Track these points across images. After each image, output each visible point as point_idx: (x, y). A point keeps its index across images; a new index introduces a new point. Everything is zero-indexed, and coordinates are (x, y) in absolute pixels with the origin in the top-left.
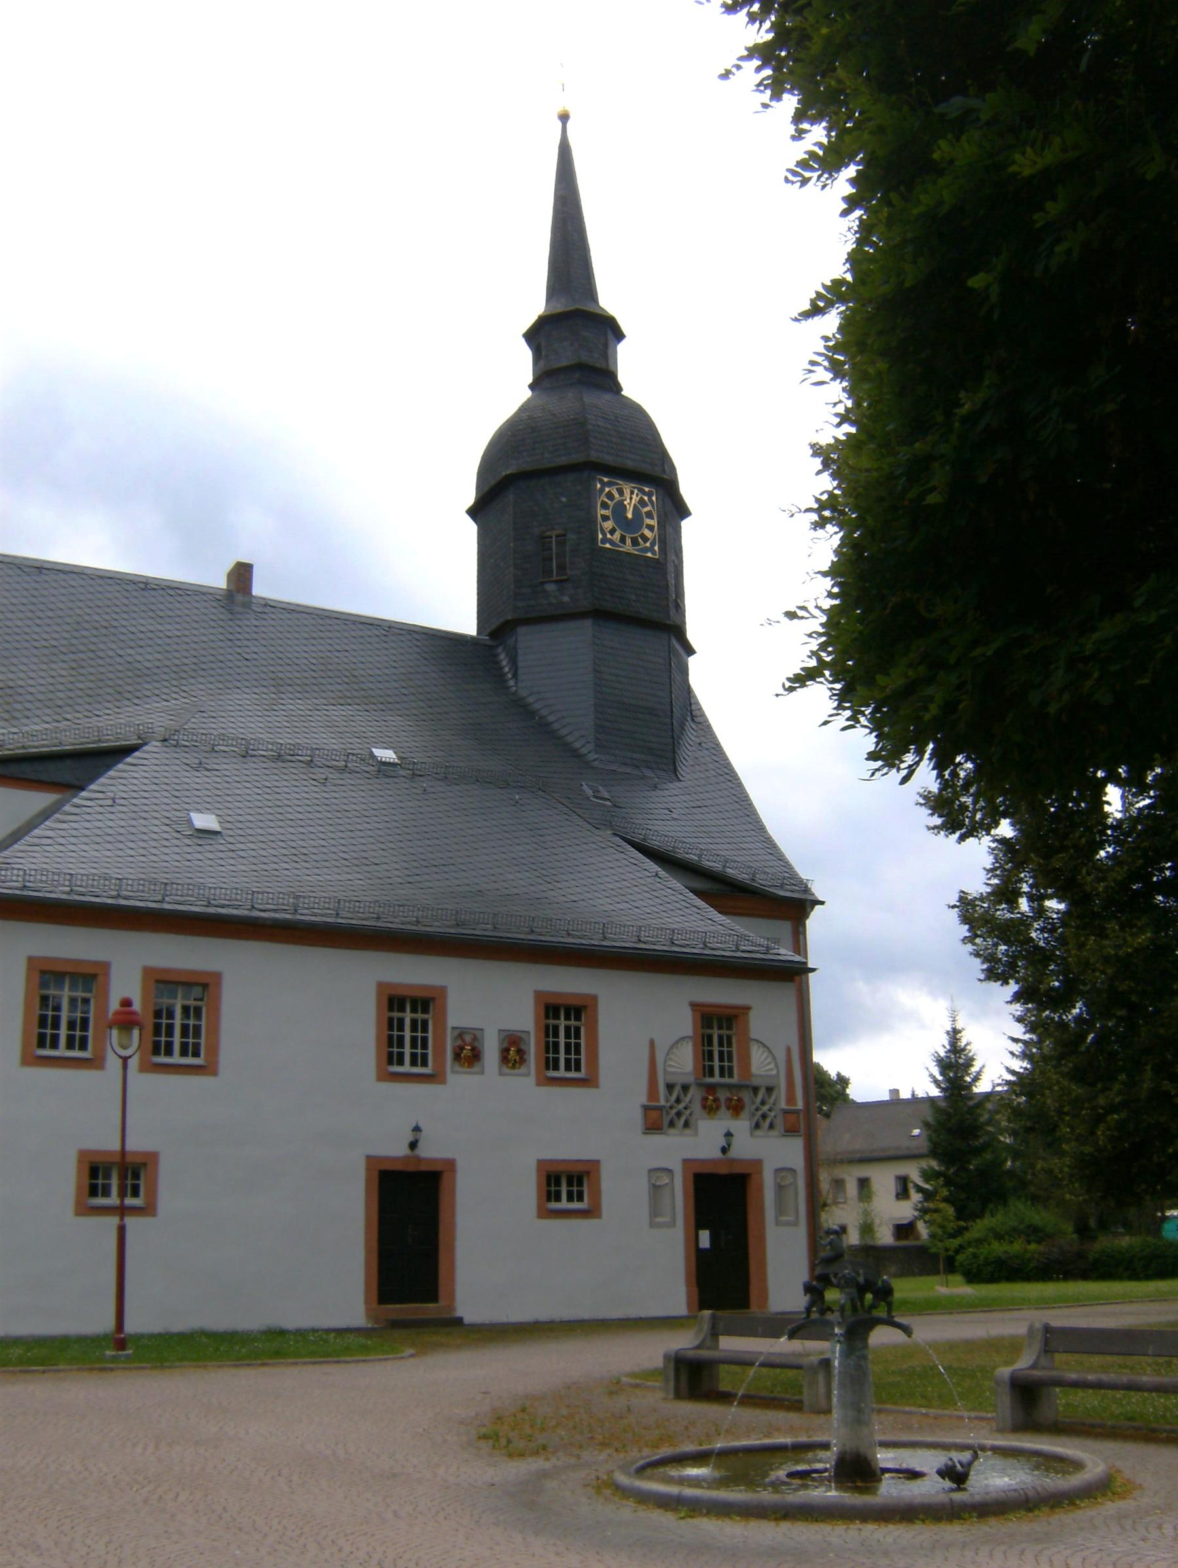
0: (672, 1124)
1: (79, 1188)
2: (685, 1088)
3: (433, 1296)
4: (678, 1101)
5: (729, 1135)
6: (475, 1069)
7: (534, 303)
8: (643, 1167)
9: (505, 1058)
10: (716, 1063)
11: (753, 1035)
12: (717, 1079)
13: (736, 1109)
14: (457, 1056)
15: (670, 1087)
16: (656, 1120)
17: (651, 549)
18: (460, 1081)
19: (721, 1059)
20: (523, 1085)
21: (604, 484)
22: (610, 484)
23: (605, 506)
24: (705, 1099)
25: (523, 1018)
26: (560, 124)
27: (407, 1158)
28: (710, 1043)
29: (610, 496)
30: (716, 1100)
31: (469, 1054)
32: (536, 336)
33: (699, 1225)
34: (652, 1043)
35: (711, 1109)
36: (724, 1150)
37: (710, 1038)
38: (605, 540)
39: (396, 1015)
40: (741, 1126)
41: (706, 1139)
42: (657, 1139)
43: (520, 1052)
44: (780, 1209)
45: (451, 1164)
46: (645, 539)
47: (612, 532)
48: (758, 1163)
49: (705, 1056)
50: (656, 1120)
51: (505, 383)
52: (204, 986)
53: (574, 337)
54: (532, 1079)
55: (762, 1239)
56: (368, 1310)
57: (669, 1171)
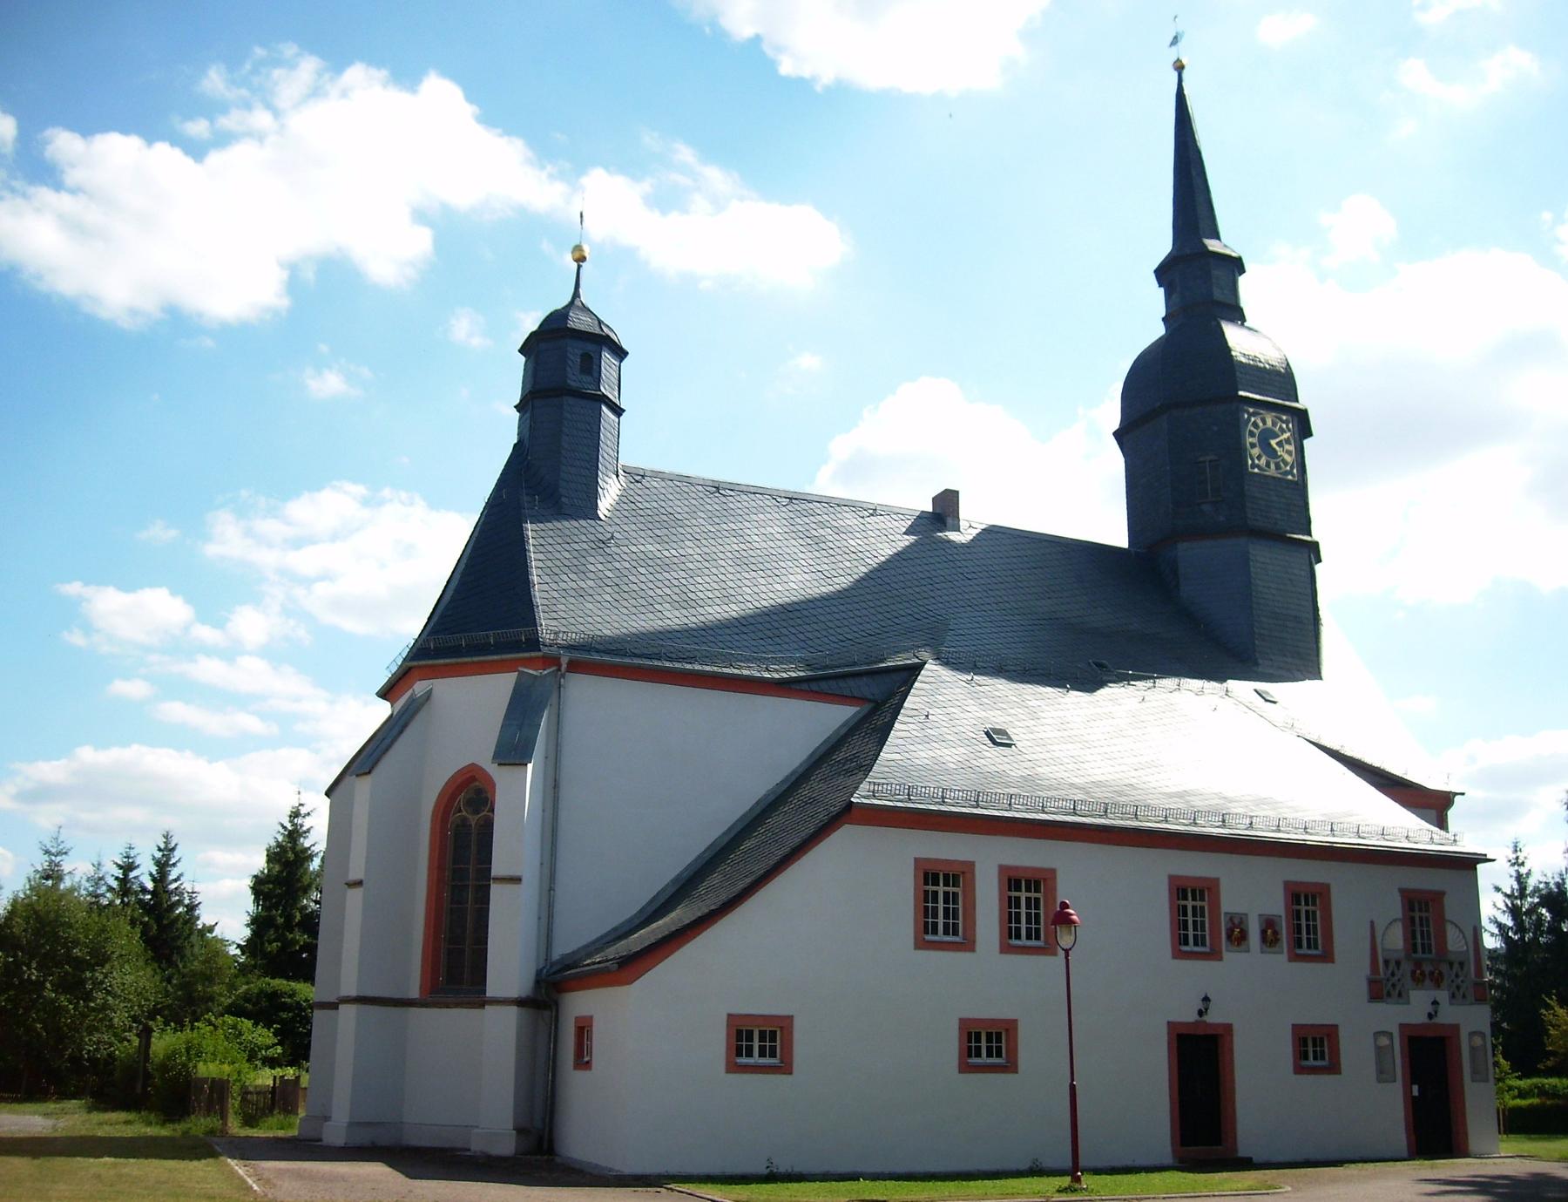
0: (1389, 995)
1: (728, 1049)
2: (1398, 963)
3: (1218, 1141)
4: (1393, 974)
5: (1435, 1003)
6: (1243, 947)
7: (1163, 244)
8: (1368, 1028)
9: (1010, 931)
10: (1191, 932)
11: (1448, 916)
12: (1420, 955)
13: (1437, 981)
14: (1229, 937)
15: (1386, 962)
16: (1378, 991)
17: (1290, 472)
18: (1231, 957)
19: (1195, 929)
20: (1279, 960)
21: (1251, 415)
22: (1254, 414)
23: (1252, 434)
24: (1413, 973)
25: (1276, 905)
26: (1176, 74)
27: (1196, 1024)
28: (1299, 918)
29: (1255, 425)
30: (1422, 973)
31: (1238, 936)
32: (1164, 273)
33: (1413, 1083)
34: (1372, 923)
35: (1418, 979)
36: (1430, 1016)
37: (1298, 912)
38: (1254, 466)
39: (931, 888)
40: (1443, 996)
41: (1416, 1007)
42: (1380, 1007)
43: (1275, 933)
44: (1475, 1072)
45: (1228, 1028)
46: (1286, 464)
47: (1259, 458)
48: (1455, 1028)
49: (1410, 936)
50: (1378, 991)
51: (1144, 319)
52: (1437, 897)
53: (1199, 278)
54: (1284, 957)
55: (1462, 1093)
56: (1174, 1151)
57: (1390, 1035)
